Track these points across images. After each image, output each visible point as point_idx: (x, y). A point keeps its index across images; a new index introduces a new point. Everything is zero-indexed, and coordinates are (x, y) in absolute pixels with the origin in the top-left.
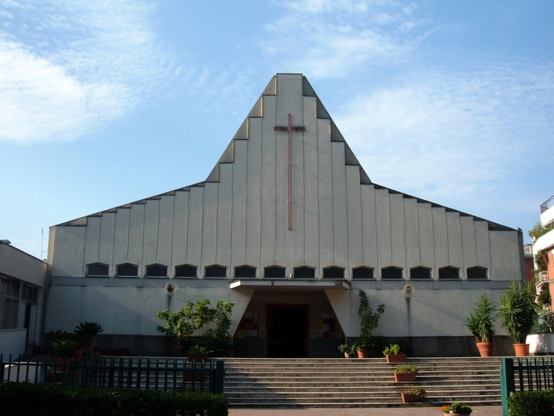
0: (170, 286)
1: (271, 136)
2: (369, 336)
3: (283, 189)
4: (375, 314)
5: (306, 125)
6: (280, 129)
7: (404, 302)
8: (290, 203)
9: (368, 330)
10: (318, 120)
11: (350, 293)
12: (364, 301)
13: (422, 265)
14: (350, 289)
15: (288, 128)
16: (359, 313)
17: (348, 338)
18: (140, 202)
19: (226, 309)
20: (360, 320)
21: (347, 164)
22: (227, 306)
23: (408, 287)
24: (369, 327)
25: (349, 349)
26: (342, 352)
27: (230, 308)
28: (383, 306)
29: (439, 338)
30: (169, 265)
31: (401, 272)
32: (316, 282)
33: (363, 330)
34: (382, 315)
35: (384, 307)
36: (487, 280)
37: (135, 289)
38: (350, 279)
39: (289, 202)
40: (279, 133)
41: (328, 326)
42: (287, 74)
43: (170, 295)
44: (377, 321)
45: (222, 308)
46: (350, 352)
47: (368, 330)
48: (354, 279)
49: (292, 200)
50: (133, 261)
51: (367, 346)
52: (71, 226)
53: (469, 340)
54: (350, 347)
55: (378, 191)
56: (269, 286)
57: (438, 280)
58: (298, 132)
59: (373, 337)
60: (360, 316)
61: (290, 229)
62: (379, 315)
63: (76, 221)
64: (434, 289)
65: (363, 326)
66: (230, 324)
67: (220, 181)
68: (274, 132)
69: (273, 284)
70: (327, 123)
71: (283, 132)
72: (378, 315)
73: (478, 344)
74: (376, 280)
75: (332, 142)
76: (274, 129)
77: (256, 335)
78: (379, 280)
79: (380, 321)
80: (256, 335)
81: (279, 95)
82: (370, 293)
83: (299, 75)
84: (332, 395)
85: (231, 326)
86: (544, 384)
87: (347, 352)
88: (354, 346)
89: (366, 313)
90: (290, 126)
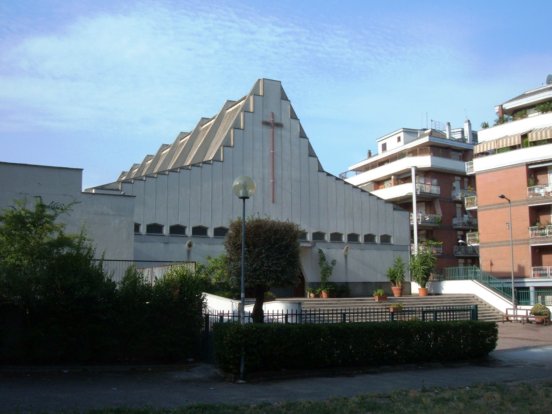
0: (190, 243)
1: (260, 129)
3: (268, 171)
5: (283, 122)
6: (266, 123)
7: (343, 258)
10: (291, 119)
12: (323, 258)
13: (355, 232)
18: (162, 173)
21: (310, 156)
23: (348, 248)
28: (335, 261)
29: (364, 283)
30: (188, 226)
31: (139, 227)
36: (163, 235)
37: (162, 245)
40: (265, 126)
42: (270, 80)
43: (189, 250)
48: (148, 234)
50: (159, 222)
52: (105, 189)
53: (380, 285)
55: (329, 177)
56: (544, 255)
57: (364, 243)
58: (278, 128)
63: (110, 186)
64: (361, 250)
68: (261, 125)
71: (267, 126)
73: (393, 288)
79: (333, 271)
82: (325, 251)
83: (278, 82)
84: (485, 313)
86: (340, 318)
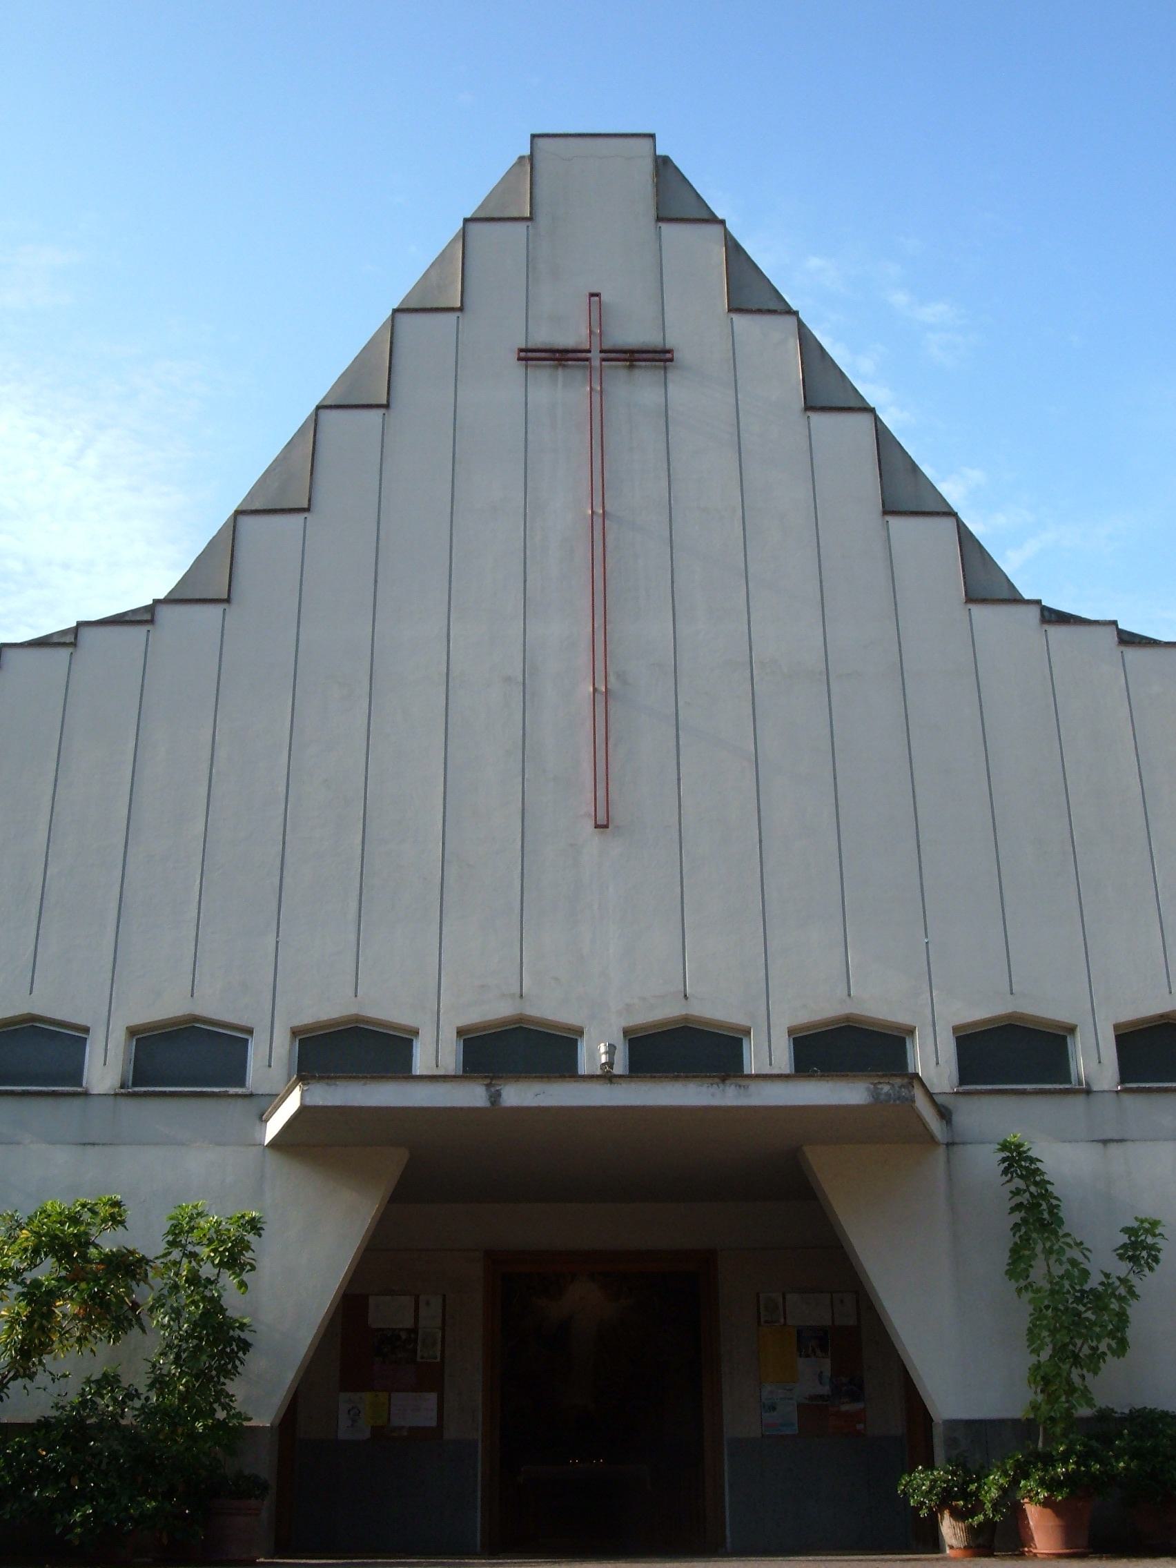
2: (1084, 1411)
4: (1107, 1276)
8: (603, 697)
9: (1075, 1374)
11: (948, 1161)
14: (949, 1145)
15: (589, 351)
16: (1012, 1273)
17: (952, 1424)
19: (215, 1250)
20: (1021, 1313)
22: (217, 1238)
24: (1076, 1360)
25: (965, 1495)
26: (924, 1513)
27: (241, 1245)
32: (754, 1087)
33: (1044, 1379)
34: (1146, 1283)
35: (1154, 1235)
38: (948, 1090)
39: (595, 690)
41: (826, 1365)
44: (1122, 1319)
45: (197, 1249)
46: (972, 1513)
47: (1075, 1374)
49: (612, 679)
51: (1088, 1472)
54: (972, 1482)
59: (1104, 1416)
60: (1019, 1290)
61: (602, 820)
62: (1134, 1279)
65: (1036, 1351)
66: (245, 1346)
67: (234, 596)
69: (495, 1097)
70: (779, 331)
72: (1123, 1281)
74: (1088, 1092)
75: (809, 413)
76: (519, 359)
77: (434, 1423)
78: (1106, 1088)
80: (434, 1423)
81: (543, 220)
85: (255, 1363)
87: (958, 1515)
88: (1005, 1473)
89: (1058, 1270)
90: (596, 340)
